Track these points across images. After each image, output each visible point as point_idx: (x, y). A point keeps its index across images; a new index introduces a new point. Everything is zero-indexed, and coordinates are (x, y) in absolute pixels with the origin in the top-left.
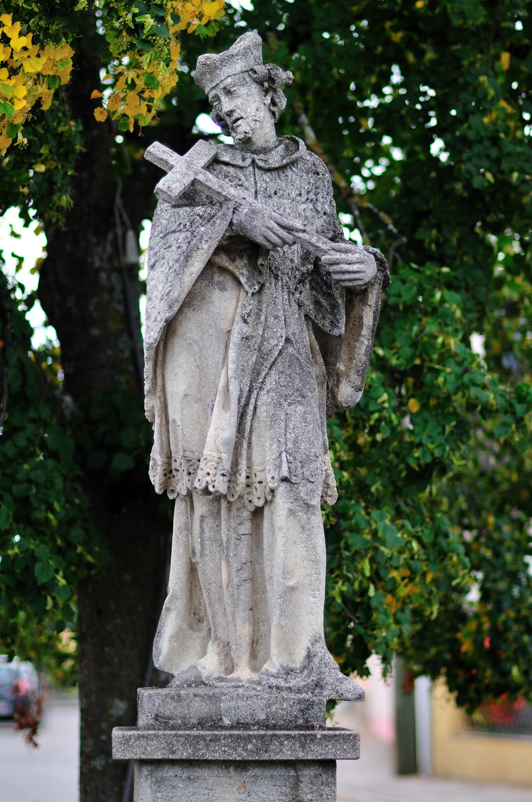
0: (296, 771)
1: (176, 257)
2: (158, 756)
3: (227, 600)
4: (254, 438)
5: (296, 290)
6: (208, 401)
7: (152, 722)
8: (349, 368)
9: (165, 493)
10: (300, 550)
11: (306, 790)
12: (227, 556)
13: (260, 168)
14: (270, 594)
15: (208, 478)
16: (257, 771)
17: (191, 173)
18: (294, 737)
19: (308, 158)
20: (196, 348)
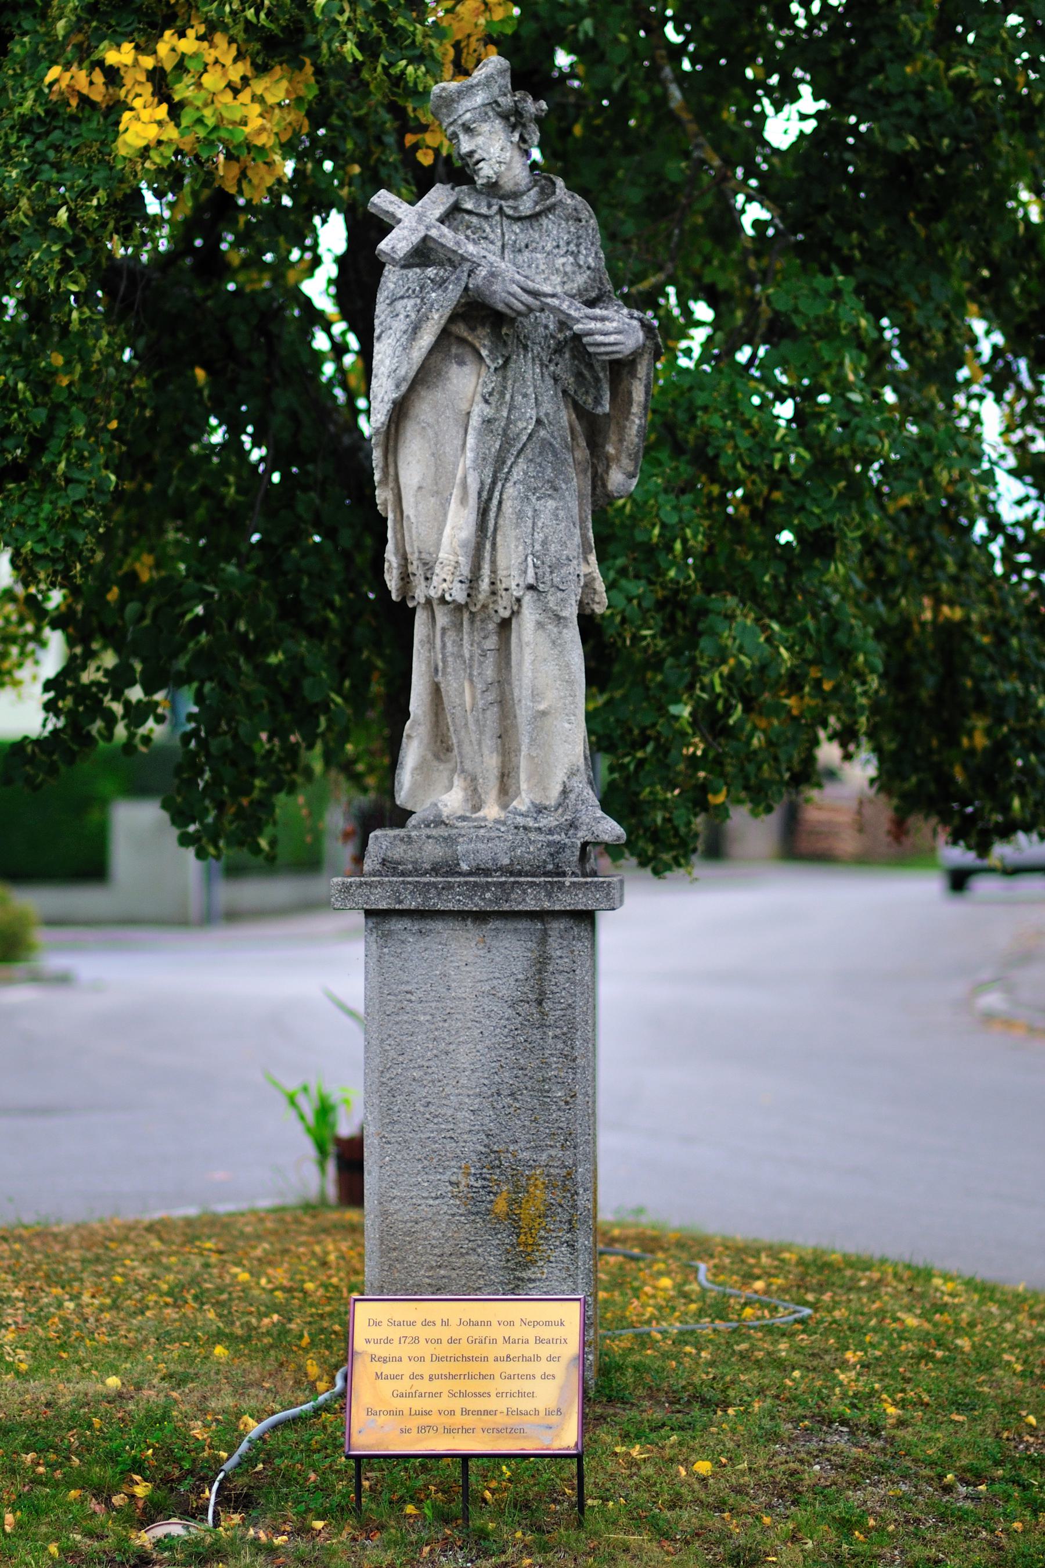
0: (543, 923)
1: (404, 327)
2: (383, 905)
3: (472, 727)
4: (499, 538)
5: (550, 361)
6: (446, 494)
7: (378, 867)
8: (619, 451)
9: (404, 600)
10: (551, 669)
11: (555, 945)
12: (471, 675)
13: (508, 217)
14: (519, 720)
15: (445, 585)
16: (498, 924)
17: (422, 228)
18: (538, 885)
19: (569, 201)
20: (430, 432)
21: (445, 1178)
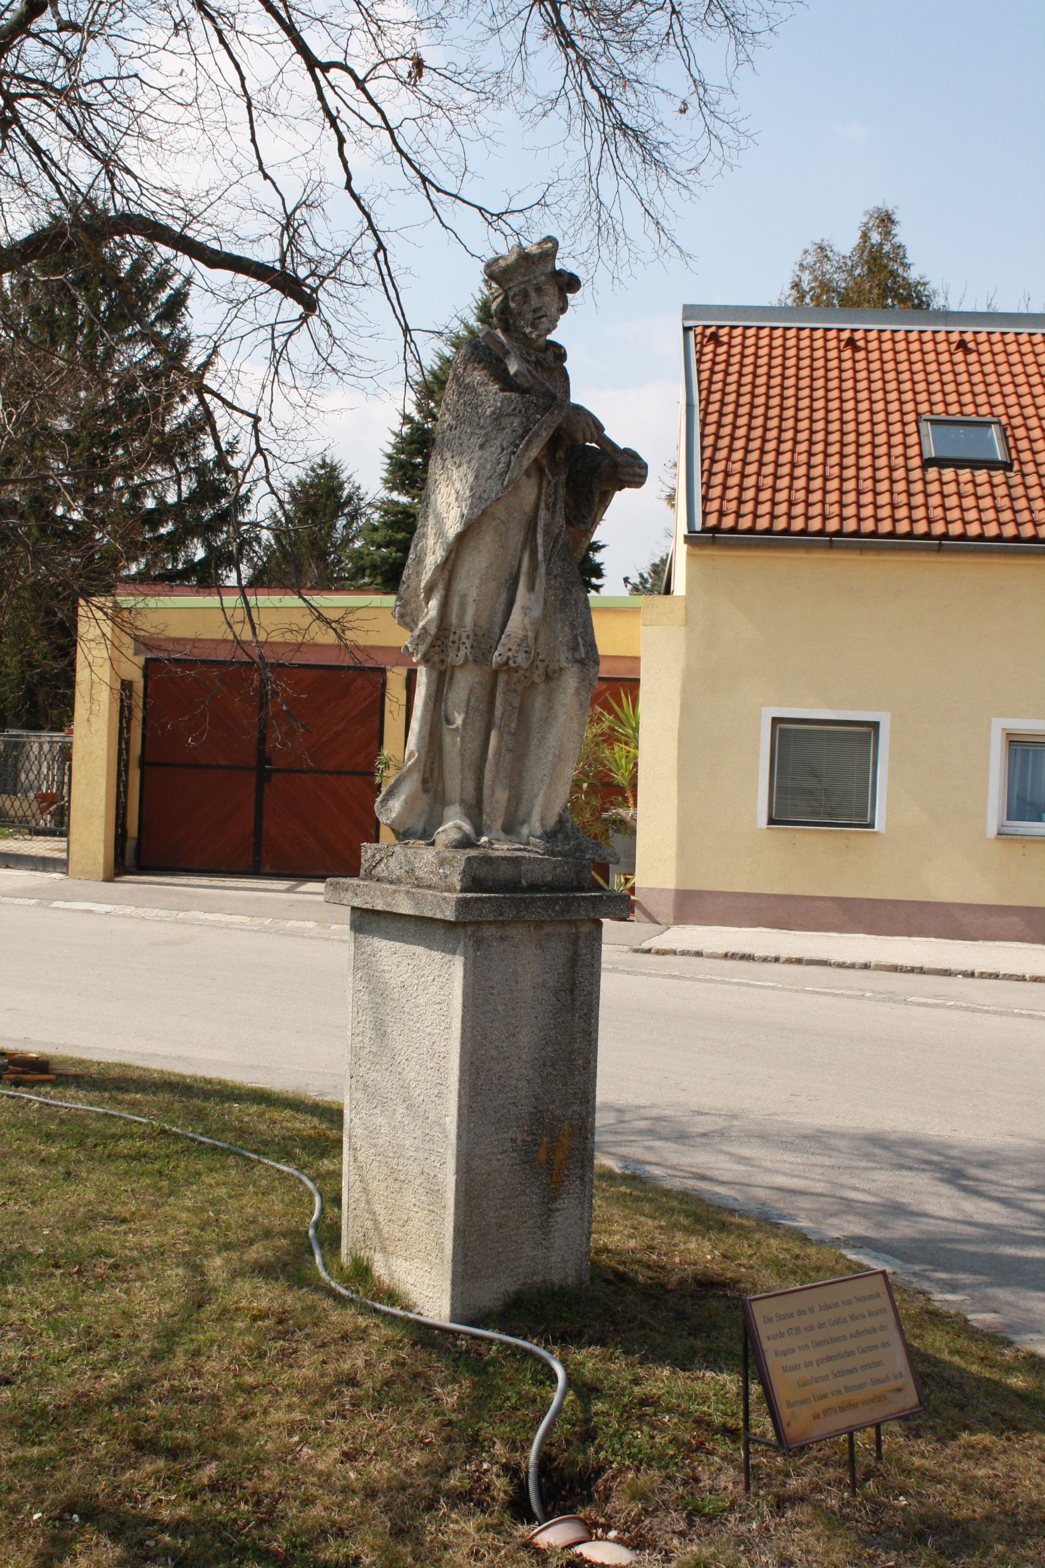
21: (508, 1136)
